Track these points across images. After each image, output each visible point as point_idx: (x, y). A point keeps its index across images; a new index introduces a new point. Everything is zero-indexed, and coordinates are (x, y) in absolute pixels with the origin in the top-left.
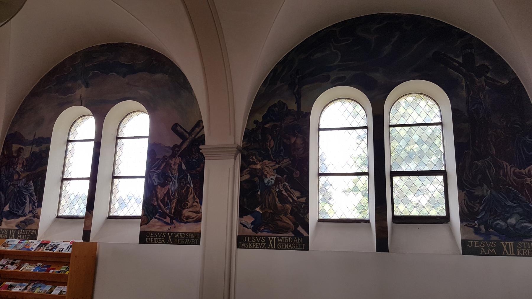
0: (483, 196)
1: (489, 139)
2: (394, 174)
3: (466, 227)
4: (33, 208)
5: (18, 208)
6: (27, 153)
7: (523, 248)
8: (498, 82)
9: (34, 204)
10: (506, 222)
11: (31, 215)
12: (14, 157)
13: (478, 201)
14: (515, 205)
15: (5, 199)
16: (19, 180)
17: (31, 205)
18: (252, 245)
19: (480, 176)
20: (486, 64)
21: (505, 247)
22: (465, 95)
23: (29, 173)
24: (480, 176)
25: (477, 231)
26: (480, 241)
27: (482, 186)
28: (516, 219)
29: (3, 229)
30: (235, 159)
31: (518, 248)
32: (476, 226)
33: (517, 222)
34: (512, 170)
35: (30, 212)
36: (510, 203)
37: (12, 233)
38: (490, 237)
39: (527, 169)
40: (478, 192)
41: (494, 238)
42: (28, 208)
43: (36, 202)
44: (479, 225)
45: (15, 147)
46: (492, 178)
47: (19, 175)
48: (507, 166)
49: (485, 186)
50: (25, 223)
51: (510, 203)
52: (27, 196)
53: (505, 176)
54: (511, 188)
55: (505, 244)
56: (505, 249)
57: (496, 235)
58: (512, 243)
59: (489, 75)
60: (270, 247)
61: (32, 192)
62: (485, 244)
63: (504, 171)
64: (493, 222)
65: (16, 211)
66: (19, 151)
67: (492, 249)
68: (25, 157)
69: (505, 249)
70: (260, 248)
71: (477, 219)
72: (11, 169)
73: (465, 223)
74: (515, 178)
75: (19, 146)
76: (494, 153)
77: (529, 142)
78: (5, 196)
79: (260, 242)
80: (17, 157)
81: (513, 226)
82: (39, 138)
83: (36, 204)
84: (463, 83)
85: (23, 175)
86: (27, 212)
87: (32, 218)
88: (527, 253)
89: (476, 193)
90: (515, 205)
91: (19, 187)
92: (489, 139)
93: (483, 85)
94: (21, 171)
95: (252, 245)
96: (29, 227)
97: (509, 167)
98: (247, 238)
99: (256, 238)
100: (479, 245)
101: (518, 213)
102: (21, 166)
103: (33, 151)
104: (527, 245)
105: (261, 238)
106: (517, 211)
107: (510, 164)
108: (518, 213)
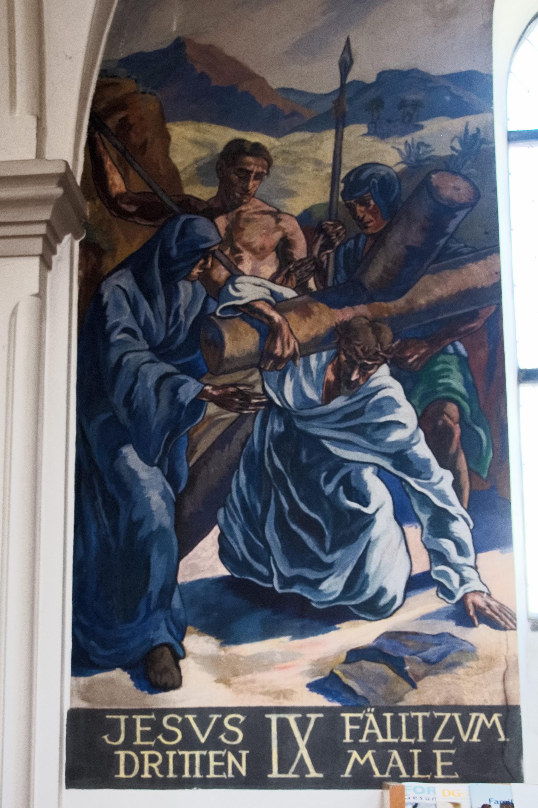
2: (40, 153)
4: (438, 557)
5: (295, 552)
6: (303, 176)
9: (440, 523)
11: (428, 601)
12: (190, 205)
15: (177, 506)
16: (266, 359)
17: (413, 532)
21: (303, 752)
23: (346, 314)
29: (202, 714)
30: (46, 263)
35: (416, 583)
42: (392, 553)
43: (456, 508)
45: (191, 144)
47: (269, 332)
50: (397, 664)
52: (368, 474)
56: (302, 743)
61: (409, 443)
65: (286, 582)
66: (234, 167)
68: (297, 206)
69: (302, 743)
72: (185, 289)
75: (222, 136)
78: (172, 477)
79: (213, 743)
80: (230, 200)
82: (386, 77)
83: (461, 529)
85: (302, 329)
86: (395, 585)
87: (450, 627)
91: (283, 412)
94: (278, 303)
96: (433, 690)
98: (131, 725)
99: (185, 726)
102: (269, 268)
103: (350, 162)
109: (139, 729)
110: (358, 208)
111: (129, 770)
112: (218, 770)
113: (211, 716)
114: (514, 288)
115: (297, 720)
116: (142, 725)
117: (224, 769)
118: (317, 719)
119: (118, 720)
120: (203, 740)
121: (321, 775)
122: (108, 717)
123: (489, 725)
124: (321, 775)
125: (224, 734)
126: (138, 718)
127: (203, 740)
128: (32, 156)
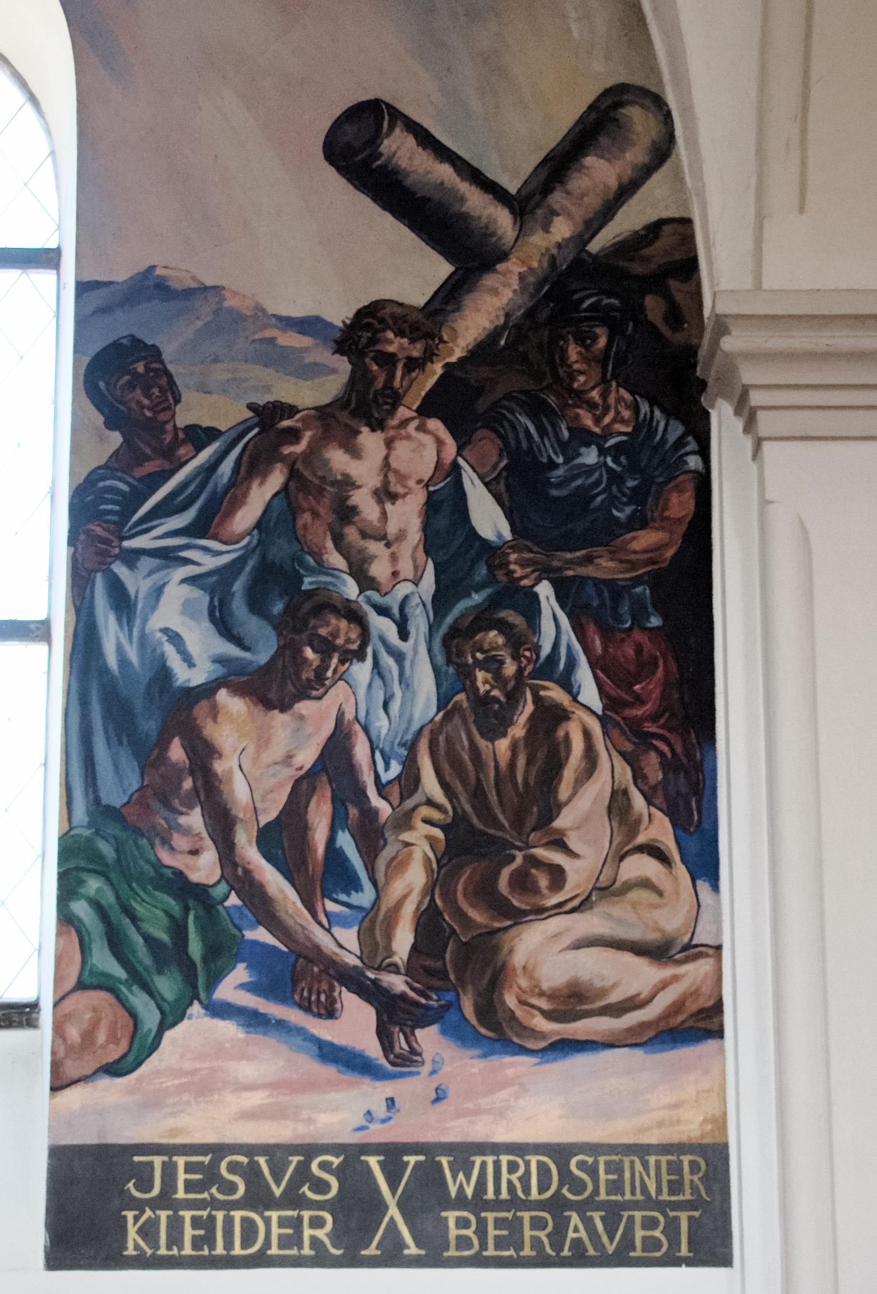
98: (169, 1171)
99: (252, 1174)
105: (303, 1172)
109: (182, 1177)
110: (480, 675)
111: (247, 1242)
112: (197, 1243)
113: (406, 1158)
114: (43, 762)
115: (449, 1162)
116: (187, 1171)
117: (298, 1242)
118: (417, 1163)
119: (151, 1164)
120: (278, 1192)
121: (423, 1252)
122: (136, 1159)
123: (461, 1176)
124: (423, 1252)
125: (217, 1186)
126: (181, 1161)
127: (278, 1192)
128: (766, 446)
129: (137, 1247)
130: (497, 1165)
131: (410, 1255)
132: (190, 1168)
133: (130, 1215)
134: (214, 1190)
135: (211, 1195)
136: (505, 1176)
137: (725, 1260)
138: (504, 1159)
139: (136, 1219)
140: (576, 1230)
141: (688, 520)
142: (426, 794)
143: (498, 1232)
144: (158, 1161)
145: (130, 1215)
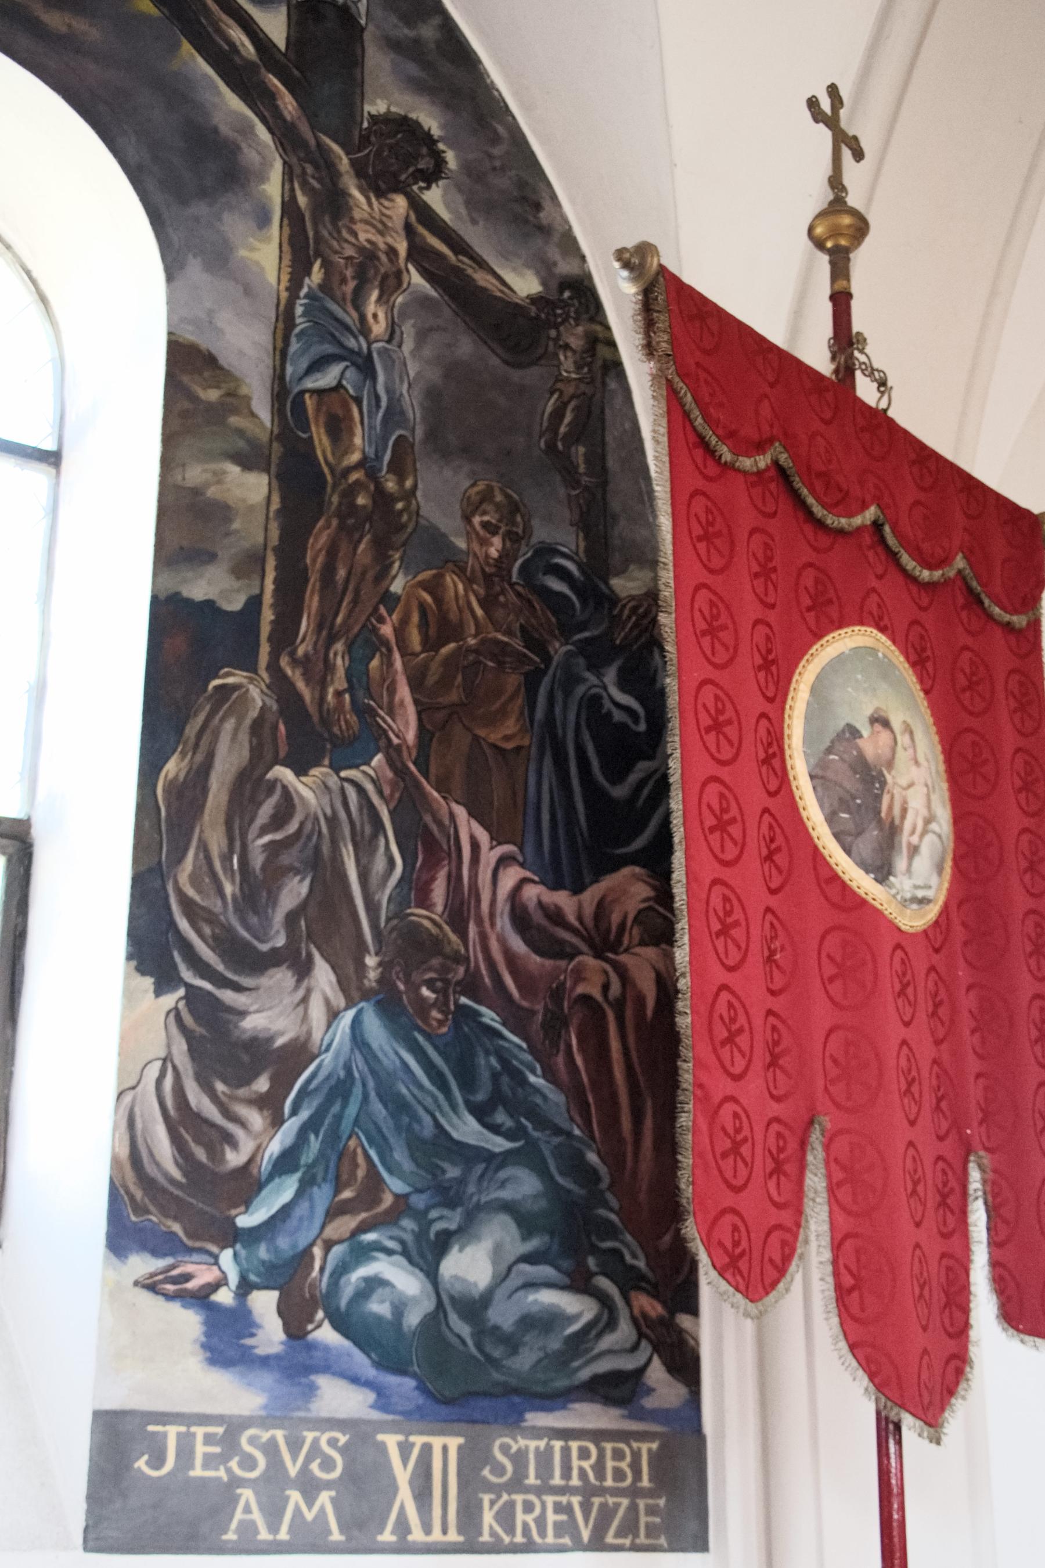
0: (299, 1053)
1: (387, 630)
3: (146, 1298)
7: (517, 1484)
8: (481, 264)
10: (432, 1274)
13: (262, 1084)
14: (499, 1144)
18: (506, 1517)
19: (295, 891)
20: (431, 122)
21: (403, 1475)
22: (272, 277)
24: (295, 891)
25: (226, 1340)
26: (234, 1426)
27: (303, 970)
28: (497, 1251)
31: (489, 1487)
32: (224, 1297)
33: (501, 1278)
34: (510, 877)
36: (467, 1129)
37: (422, 1494)
38: (312, 1390)
39: (590, 896)
40: (269, 1011)
41: (339, 1399)
44: (245, 1287)
46: (372, 908)
48: (475, 846)
49: (323, 975)
51: (467, 1129)
53: (459, 913)
54: (489, 1017)
55: (405, 1449)
57: (355, 1380)
58: (454, 1443)
59: (434, 197)
60: (403, 1527)
62: (271, 1449)
63: (454, 880)
64: (343, 1269)
67: (310, 1488)
69: (405, 1495)
70: (579, 1546)
71: (231, 1236)
73: (142, 1265)
74: (518, 945)
76: (411, 736)
77: (618, 716)
81: (473, 1308)
84: (273, 188)
88: (541, 1522)
89: (253, 1023)
90: (499, 1144)
92: (387, 630)
93: (392, 252)
95: (506, 1517)
97: (490, 856)
100: (223, 1459)
101: (507, 1207)
104: (544, 1459)
106: (506, 1194)
107: (497, 839)
108: (507, 1207)
109: (200, 1449)
127: (293, 1470)
129: (493, 1533)
130: (566, 1451)
131: (383, 1543)
132: (209, 1439)
133: (486, 1498)
134: (233, 1464)
135: (229, 1471)
136: (575, 1463)
137: (700, 1544)
138: (574, 1445)
139: (492, 1503)
140: (247, 1510)
141: (971, 1199)
142: (535, 1196)
143: (650, 1519)
144: (172, 1432)
145: (486, 1498)
